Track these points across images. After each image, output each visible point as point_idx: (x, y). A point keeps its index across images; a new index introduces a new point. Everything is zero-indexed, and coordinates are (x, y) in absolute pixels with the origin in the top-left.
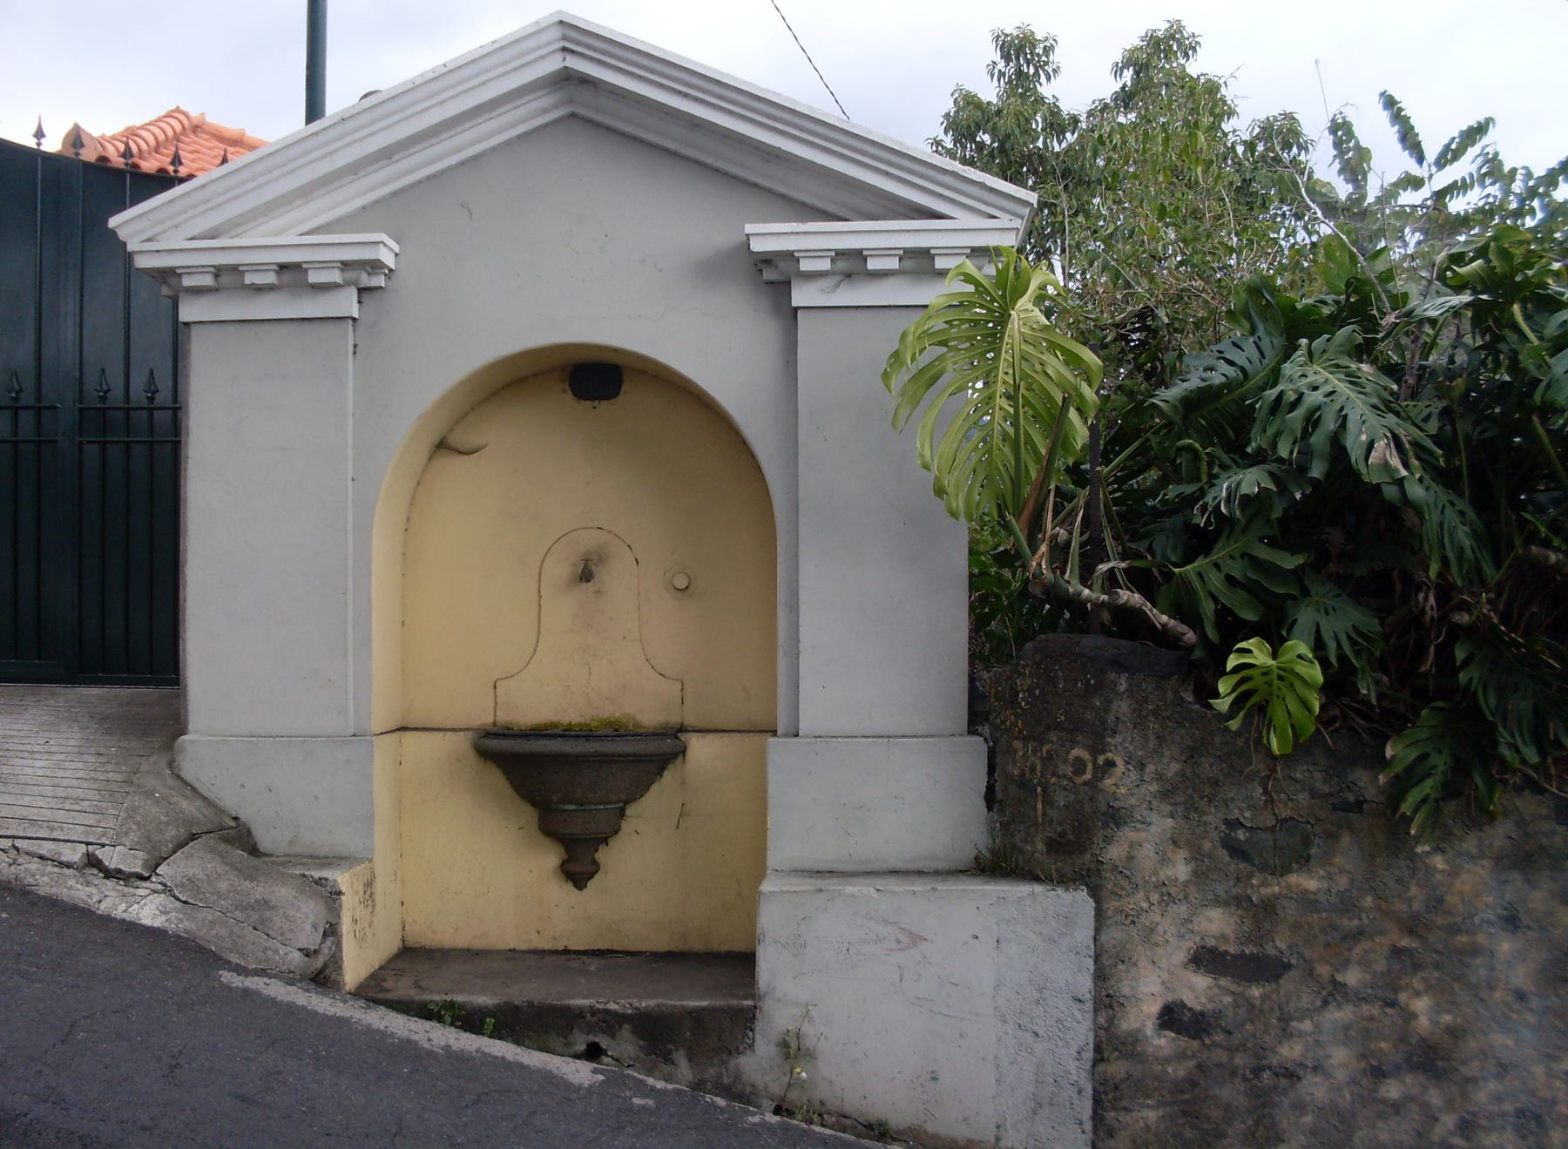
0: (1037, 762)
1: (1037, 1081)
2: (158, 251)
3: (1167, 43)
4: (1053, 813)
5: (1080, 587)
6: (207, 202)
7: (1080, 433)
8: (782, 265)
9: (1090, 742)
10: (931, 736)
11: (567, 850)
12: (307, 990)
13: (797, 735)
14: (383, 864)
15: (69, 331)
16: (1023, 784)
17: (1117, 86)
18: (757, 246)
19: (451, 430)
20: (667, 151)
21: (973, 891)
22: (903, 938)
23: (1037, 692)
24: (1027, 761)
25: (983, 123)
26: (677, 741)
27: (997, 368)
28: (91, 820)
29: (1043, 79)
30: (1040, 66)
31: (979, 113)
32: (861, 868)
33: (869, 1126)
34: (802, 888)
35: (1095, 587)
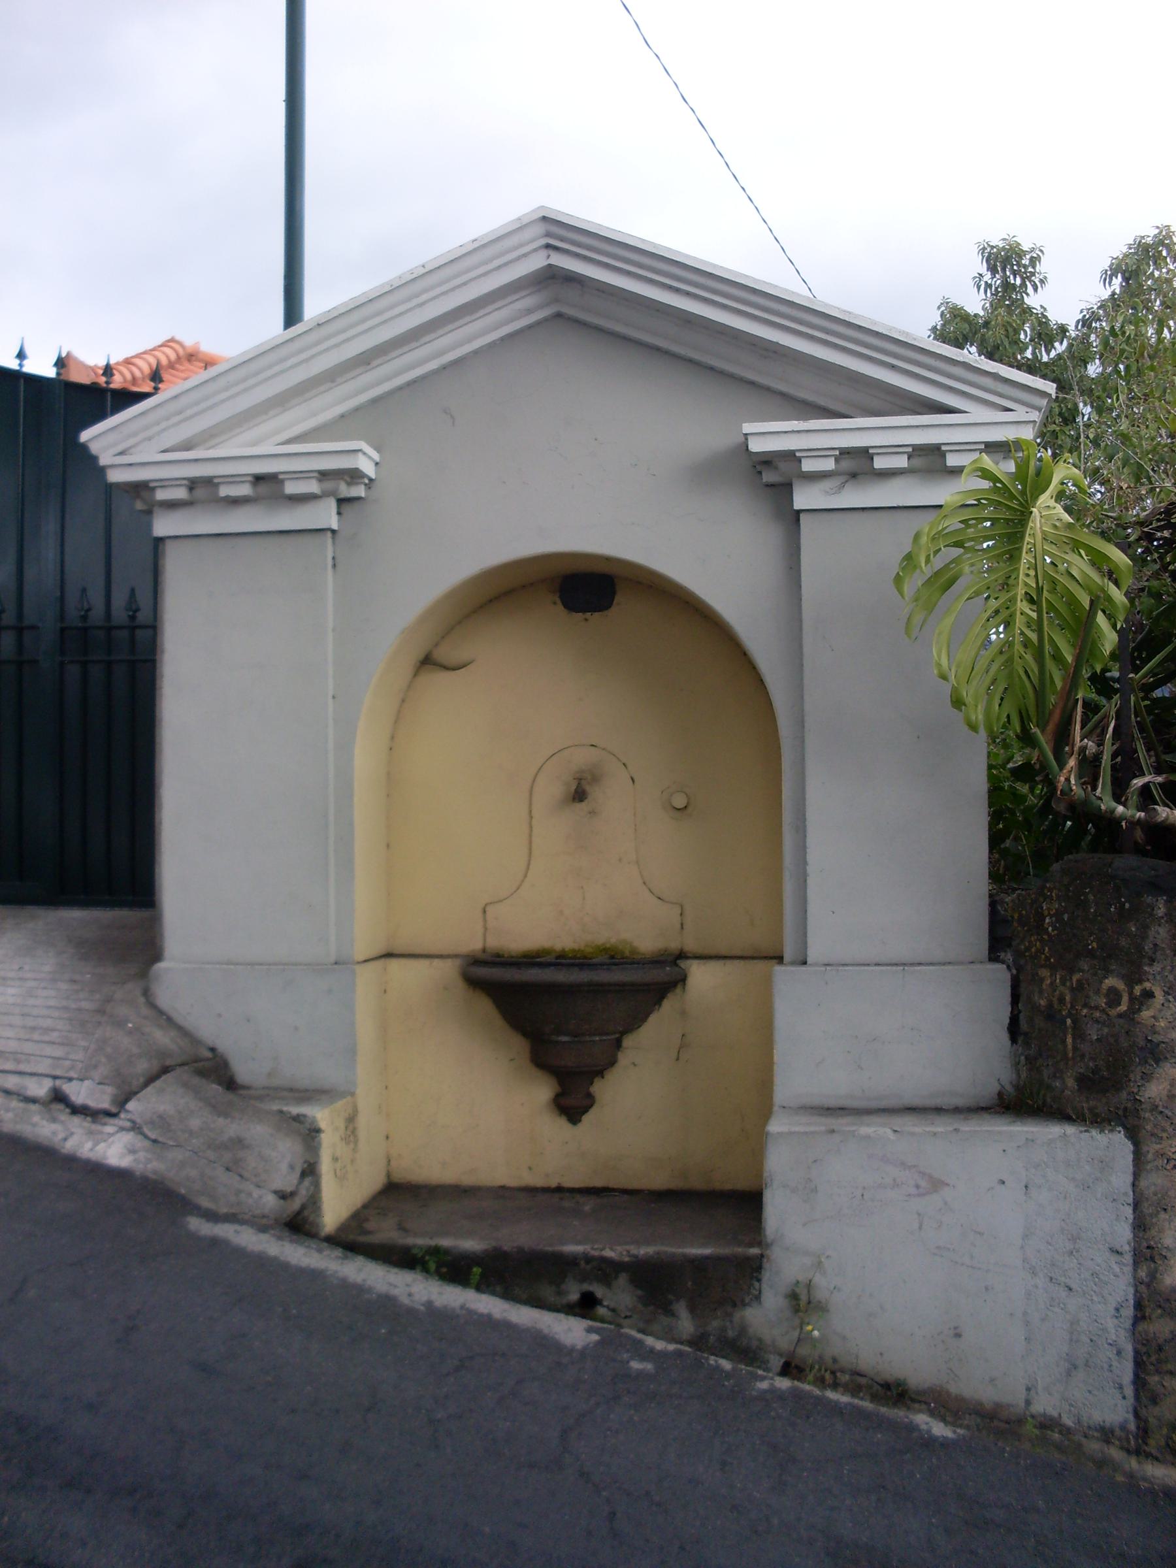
0: (1067, 992)
1: (1071, 1340)
2: (131, 465)
3: (1156, 249)
4: (1085, 1047)
5: (1114, 804)
6: (180, 413)
7: (1109, 639)
8: (783, 466)
9: (1124, 972)
10: (950, 963)
11: (561, 1083)
12: (280, 1238)
13: (805, 963)
14: (366, 1098)
15: (50, 553)
16: (1051, 1015)
17: (1106, 294)
18: (756, 446)
19: (437, 645)
20: (658, 349)
21: (1000, 1133)
22: (923, 1183)
23: (1066, 917)
24: (1055, 991)
25: (971, 335)
26: (677, 969)
27: (1017, 569)
28: (59, 1052)
29: (1030, 289)
30: (1027, 277)
31: (966, 326)
32: (874, 1104)
33: (887, 1386)
34: (812, 1129)
35: (1130, 803)
